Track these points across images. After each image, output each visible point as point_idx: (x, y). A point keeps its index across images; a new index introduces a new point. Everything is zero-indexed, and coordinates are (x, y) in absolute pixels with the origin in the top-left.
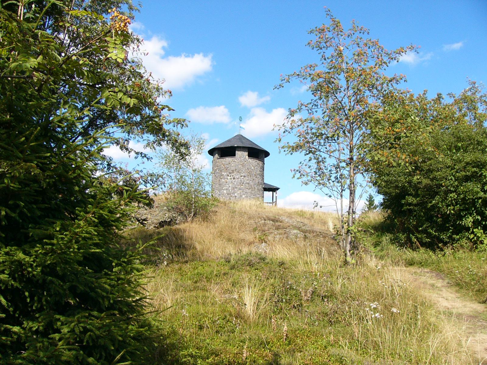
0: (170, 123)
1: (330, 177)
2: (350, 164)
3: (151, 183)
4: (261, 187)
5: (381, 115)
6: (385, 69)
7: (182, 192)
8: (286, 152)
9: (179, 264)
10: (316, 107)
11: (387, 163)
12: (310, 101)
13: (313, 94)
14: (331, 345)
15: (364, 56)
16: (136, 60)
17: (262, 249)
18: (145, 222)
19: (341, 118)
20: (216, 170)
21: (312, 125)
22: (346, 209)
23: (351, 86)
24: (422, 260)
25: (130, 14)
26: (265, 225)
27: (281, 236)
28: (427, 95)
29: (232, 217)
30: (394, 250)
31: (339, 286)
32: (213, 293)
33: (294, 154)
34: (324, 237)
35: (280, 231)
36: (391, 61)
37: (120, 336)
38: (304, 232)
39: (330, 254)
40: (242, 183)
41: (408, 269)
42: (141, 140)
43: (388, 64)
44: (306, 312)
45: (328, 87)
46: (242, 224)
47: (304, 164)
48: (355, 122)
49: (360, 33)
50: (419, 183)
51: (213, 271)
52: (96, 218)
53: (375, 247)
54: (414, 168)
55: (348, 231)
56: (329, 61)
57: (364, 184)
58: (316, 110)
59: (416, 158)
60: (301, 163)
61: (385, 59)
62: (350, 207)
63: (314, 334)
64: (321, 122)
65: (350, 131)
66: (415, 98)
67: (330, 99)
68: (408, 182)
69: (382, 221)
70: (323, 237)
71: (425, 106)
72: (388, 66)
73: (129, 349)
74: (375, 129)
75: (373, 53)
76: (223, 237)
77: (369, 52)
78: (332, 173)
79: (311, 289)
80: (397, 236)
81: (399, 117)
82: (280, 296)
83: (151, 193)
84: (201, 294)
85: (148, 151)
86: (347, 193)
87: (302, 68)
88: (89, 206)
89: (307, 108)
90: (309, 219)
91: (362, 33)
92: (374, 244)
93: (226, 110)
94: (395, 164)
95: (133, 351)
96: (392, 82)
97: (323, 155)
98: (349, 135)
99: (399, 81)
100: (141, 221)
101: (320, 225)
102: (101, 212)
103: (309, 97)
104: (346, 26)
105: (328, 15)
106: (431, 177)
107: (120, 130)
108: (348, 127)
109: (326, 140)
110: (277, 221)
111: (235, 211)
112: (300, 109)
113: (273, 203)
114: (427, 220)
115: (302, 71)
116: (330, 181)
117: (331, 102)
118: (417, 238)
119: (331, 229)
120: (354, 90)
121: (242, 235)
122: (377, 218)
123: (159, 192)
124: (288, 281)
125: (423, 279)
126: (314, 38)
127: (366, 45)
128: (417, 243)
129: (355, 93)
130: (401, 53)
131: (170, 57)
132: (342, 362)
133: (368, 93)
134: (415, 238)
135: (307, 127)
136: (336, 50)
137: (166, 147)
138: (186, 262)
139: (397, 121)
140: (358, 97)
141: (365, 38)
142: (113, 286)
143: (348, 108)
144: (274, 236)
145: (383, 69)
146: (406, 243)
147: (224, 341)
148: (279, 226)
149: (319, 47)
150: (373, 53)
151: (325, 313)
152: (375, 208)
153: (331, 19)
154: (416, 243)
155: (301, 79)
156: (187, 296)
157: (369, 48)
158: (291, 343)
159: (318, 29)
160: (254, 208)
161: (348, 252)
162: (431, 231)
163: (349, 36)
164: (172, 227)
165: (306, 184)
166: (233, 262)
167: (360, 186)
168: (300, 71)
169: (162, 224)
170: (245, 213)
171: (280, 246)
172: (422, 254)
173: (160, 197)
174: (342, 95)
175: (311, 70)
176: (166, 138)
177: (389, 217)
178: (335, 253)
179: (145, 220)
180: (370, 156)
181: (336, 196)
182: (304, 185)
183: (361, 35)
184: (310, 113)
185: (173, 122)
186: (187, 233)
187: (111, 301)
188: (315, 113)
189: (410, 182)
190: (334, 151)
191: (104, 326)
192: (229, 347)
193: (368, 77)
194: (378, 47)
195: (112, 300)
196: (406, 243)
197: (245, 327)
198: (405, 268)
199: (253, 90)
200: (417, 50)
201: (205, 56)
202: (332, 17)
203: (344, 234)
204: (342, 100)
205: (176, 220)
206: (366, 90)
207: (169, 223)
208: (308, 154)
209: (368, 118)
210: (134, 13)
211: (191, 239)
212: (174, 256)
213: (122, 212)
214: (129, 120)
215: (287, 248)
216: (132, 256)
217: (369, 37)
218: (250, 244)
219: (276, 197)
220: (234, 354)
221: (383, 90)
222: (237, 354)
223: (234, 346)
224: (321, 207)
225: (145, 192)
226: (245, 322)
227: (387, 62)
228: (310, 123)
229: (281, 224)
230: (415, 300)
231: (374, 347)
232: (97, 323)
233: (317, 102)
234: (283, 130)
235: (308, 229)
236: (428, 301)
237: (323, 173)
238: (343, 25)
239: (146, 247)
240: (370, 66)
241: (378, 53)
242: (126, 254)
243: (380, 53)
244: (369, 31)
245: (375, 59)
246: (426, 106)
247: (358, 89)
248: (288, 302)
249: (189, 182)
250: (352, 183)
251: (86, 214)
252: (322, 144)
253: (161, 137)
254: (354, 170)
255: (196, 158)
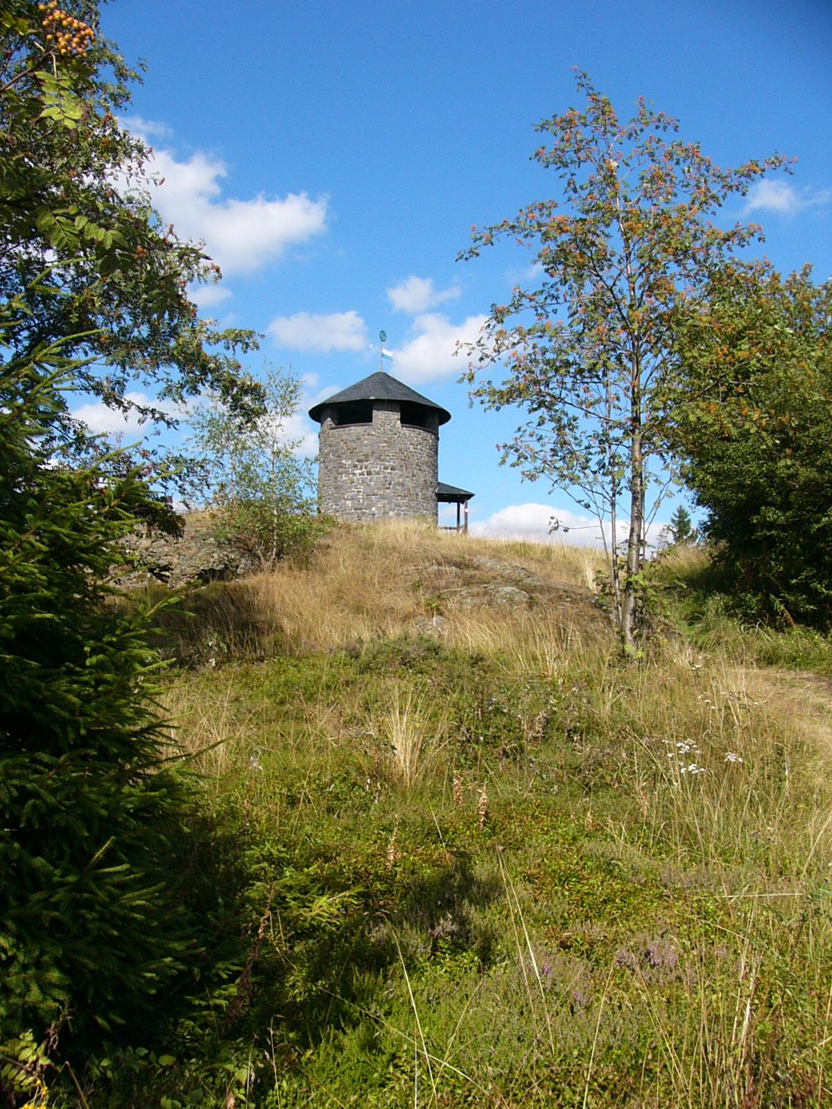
0: (218, 340)
1: (587, 462)
2: (633, 431)
3: (177, 478)
4: (430, 493)
5: (705, 319)
6: (714, 213)
7: (249, 504)
8: (487, 405)
9: (245, 665)
10: (554, 301)
11: (716, 428)
12: (541, 288)
13: (547, 271)
14: (587, 836)
15: (665, 181)
16: (135, 195)
17: (434, 627)
18: (167, 574)
19: (612, 325)
20: (328, 454)
21: (544, 342)
22: (623, 534)
23: (636, 250)
24: (797, 652)
25: (119, 88)
26: (439, 574)
27: (477, 600)
28: (811, 277)
29: (365, 557)
30: (733, 630)
31: (608, 707)
32: (320, 724)
33: (506, 408)
34: (574, 601)
35: (475, 589)
36: (729, 192)
37: (105, 807)
38: (530, 590)
39: (588, 639)
40: (387, 484)
41: (765, 672)
42: (152, 380)
43: (721, 201)
44: (532, 762)
45: (582, 254)
46: (388, 575)
47: (527, 433)
48: (644, 335)
49: (657, 127)
50: (791, 477)
51: (320, 678)
52: (43, 543)
53: (690, 625)
54: (778, 442)
55: (629, 584)
56: (584, 194)
57: (665, 476)
58: (555, 307)
59: (784, 419)
60: (519, 429)
61: (715, 189)
62: (632, 530)
63: (550, 811)
64: (566, 335)
65: (634, 356)
66: (782, 285)
67: (587, 283)
68: (766, 476)
69: (707, 565)
70: (571, 602)
71: (806, 303)
72: (720, 205)
73: (126, 836)
74: (690, 351)
75: (687, 174)
76: (343, 602)
77: (677, 173)
78: (590, 454)
79: (542, 714)
80: (741, 600)
81: (745, 324)
82: (473, 729)
83: (178, 507)
84: (292, 727)
85: (168, 407)
86: (625, 499)
87: (521, 211)
88: (28, 516)
89: (533, 303)
90: (540, 561)
91: (661, 129)
92: (689, 617)
93: (360, 322)
94: (734, 432)
95: (134, 842)
96: (730, 243)
97: (572, 411)
98: (630, 365)
99: (747, 239)
100: (157, 571)
101: (564, 575)
102: (55, 528)
103: (535, 274)
104: (624, 113)
105: (583, 86)
106: (818, 463)
107: (101, 358)
108: (629, 346)
109: (578, 377)
110: (467, 567)
111: (372, 545)
112: (517, 306)
113: (458, 528)
114: (808, 562)
115: (522, 219)
116: (587, 471)
117: (589, 289)
118: (785, 602)
119: (592, 586)
120: (642, 261)
121: (387, 599)
122: (695, 560)
123: (198, 505)
124: (491, 695)
125: (798, 693)
126: (551, 142)
127: (671, 157)
128: (787, 614)
129: (645, 269)
130: (752, 174)
131: (231, 202)
132: (611, 871)
133: (673, 268)
134: (781, 602)
135: (534, 348)
136: (601, 167)
137: (209, 401)
138: (261, 659)
139: (740, 335)
140: (652, 277)
141: (669, 138)
142: (87, 699)
143: (628, 302)
144: (460, 600)
145: (709, 212)
146: (760, 615)
147: (345, 828)
148: (471, 577)
149: (561, 162)
150: (687, 174)
151: (574, 766)
152: (693, 538)
153: (589, 95)
154: (782, 615)
155: (521, 237)
156: (261, 732)
157: (677, 163)
158: (497, 830)
159: (558, 119)
160: (416, 538)
161: (628, 632)
162: (819, 586)
163: (631, 135)
164: (227, 584)
165: (532, 478)
166: (364, 658)
167: (656, 481)
168: (518, 218)
169: (206, 576)
170: (394, 548)
171: (474, 622)
172: (796, 639)
173: (200, 516)
174: (614, 272)
175: (542, 215)
176: (210, 377)
177: (722, 556)
178: (599, 637)
179: (166, 568)
180: (677, 412)
181: (600, 505)
182: (527, 481)
183: (659, 133)
184: (541, 314)
185: (225, 337)
186: (261, 596)
187: (83, 732)
188: (551, 315)
189: (770, 476)
190: (597, 401)
191: (65, 784)
192: (355, 843)
193: (674, 230)
194: (697, 160)
195: (85, 728)
196: (760, 615)
197: (393, 798)
198: (756, 671)
199: (422, 275)
200: (789, 166)
201: (313, 199)
202: (591, 92)
203: (619, 593)
204: (614, 284)
205: (237, 567)
206: (670, 261)
207: (220, 575)
208: (535, 409)
209: (673, 326)
210: (130, 86)
211: (272, 610)
212: (233, 647)
213: (103, 529)
214: (124, 335)
215: (489, 628)
216: (128, 630)
217: (677, 137)
218: (406, 618)
219: (466, 514)
220: (368, 855)
221: (709, 262)
222: (374, 855)
223: (368, 839)
224: (566, 530)
225: (164, 499)
226: (393, 787)
227: (720, 195)
228: (541, 337)
229: (476, 572)
230: (778, 736)
231: (685, 839)
232: (51, 778)
233: (557, 290)
234: (477, 354)
235: (538, 583)
236: (808, 741)
237: (572, 453)
238: (616, 111)
239: (160, 611)
240: (678, 205)
241: (698, 176)
242: (115, 627)
243: (702, 175)
244: (678, 124)
245: (691, 189)
246: (810, 302)
247: (651, 260)
248: (492, 741)
249: (265, 480)
250: (638, 475)
251: (19, 533)
252: (569, 386)
253: (198, 373)
254: (641, 445)
255: (280, 425)
